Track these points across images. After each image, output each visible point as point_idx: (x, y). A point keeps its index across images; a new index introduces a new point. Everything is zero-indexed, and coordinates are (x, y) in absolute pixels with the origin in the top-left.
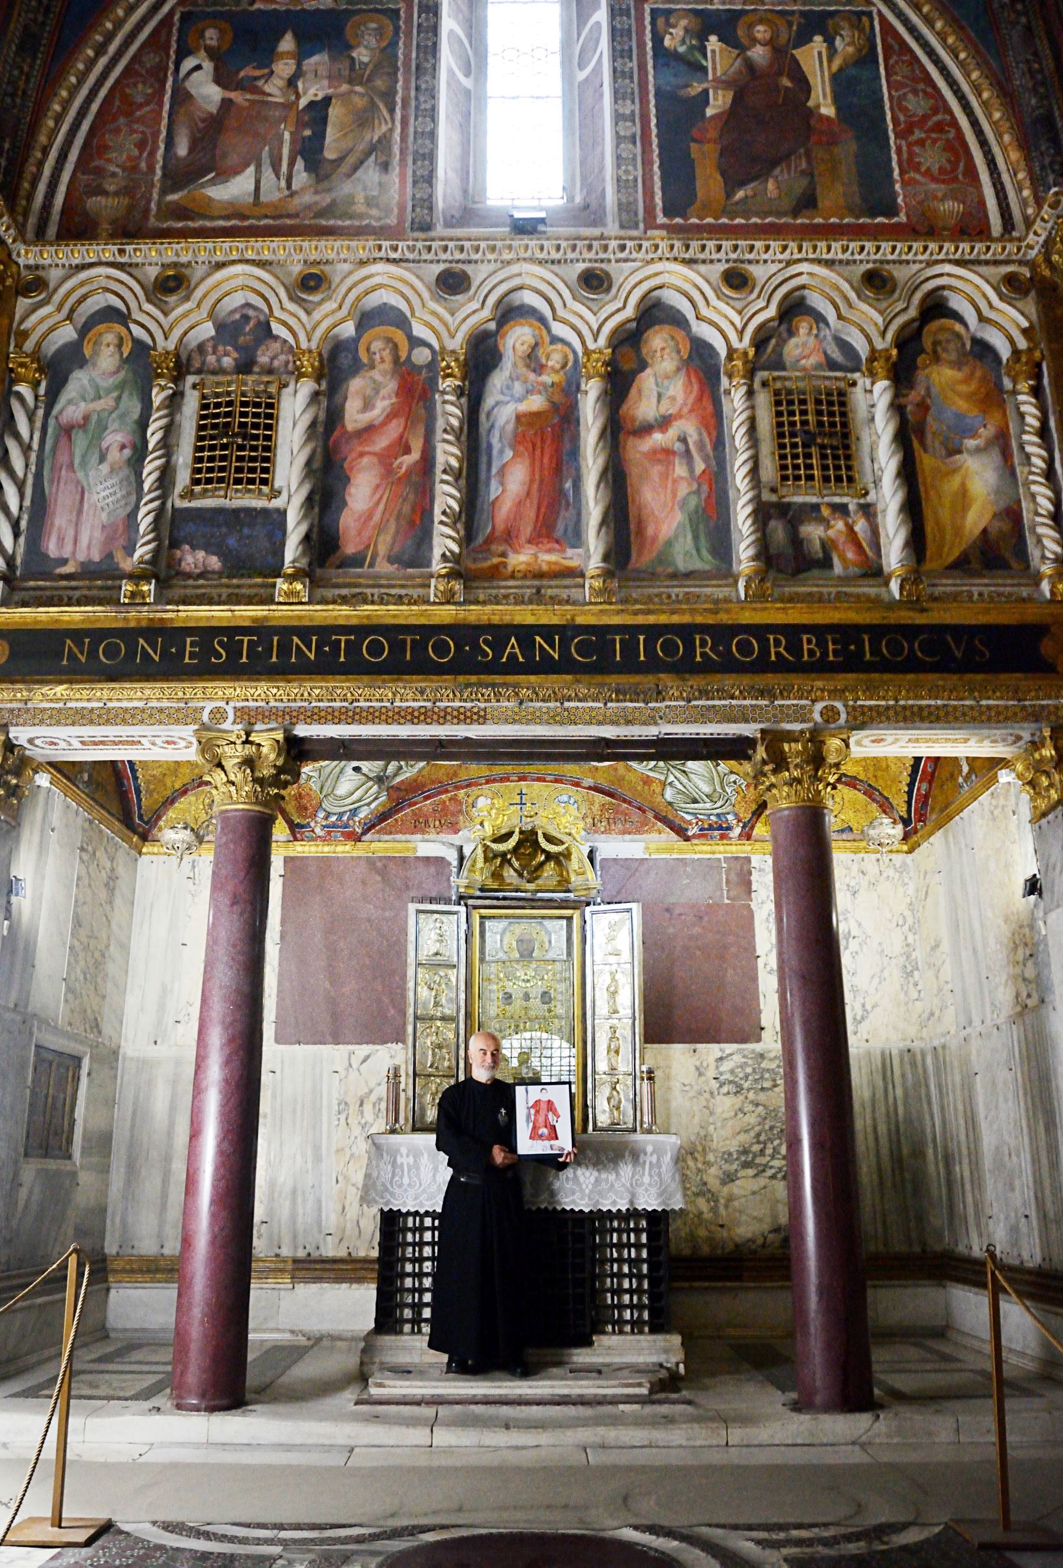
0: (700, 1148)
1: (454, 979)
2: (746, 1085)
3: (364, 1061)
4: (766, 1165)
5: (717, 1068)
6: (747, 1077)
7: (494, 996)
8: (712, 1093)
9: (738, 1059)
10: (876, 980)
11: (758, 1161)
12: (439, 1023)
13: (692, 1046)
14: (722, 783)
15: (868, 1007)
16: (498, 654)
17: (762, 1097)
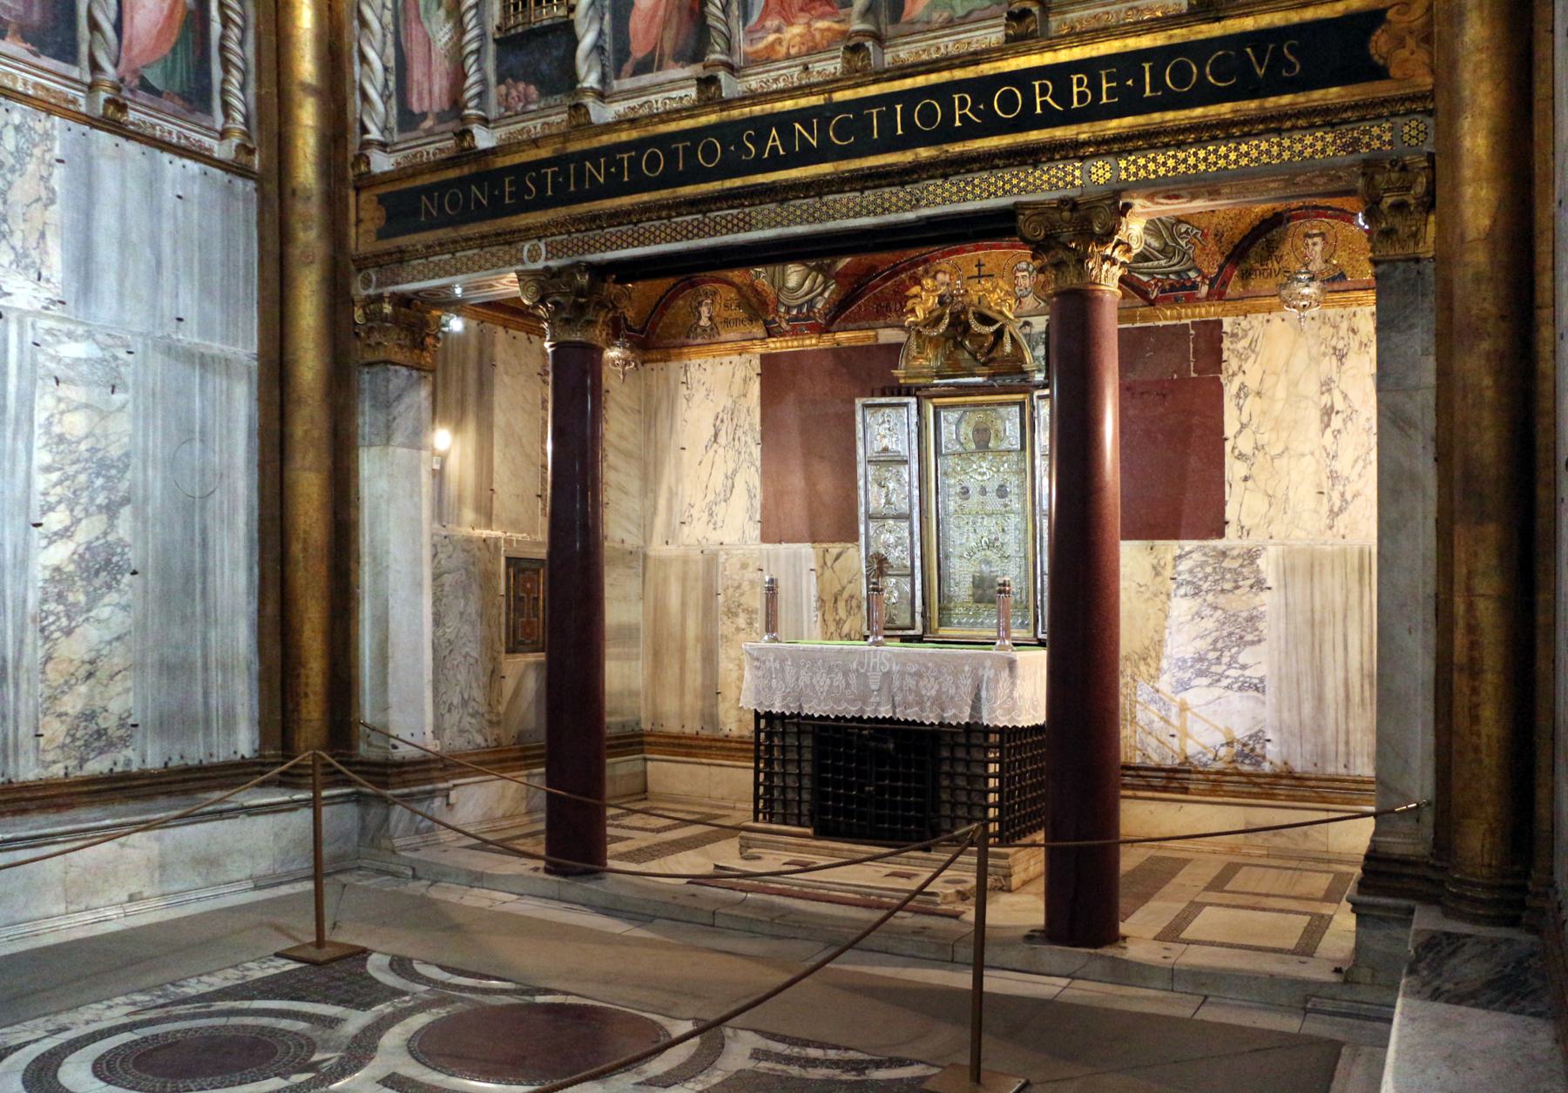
0: (1153, 654)
1: (906, 477)
2: (1205, 586)
3: (837, 559)
4: (1221, 675)
5: (1175, 567)
6: (1206, 577)
7: (952, 492)
8: (1168, 595)
9: (1197, 556)
10: (1360, 463)
11: (1214, 669)
12: (891, 522)
13: (1149, 543)
14: (1172, 235)
15: (1348, 496)
16: (760, 151)
17: (1222, 600)
